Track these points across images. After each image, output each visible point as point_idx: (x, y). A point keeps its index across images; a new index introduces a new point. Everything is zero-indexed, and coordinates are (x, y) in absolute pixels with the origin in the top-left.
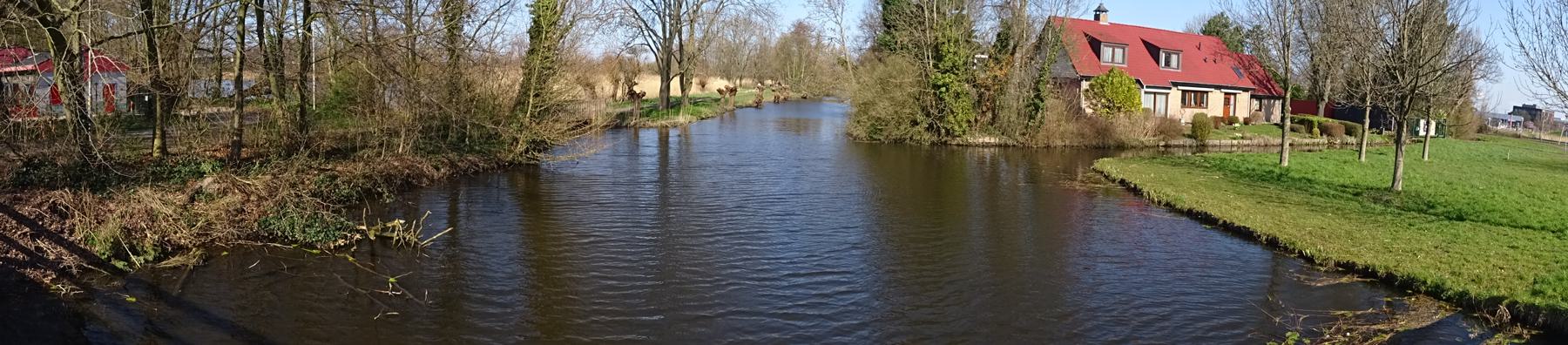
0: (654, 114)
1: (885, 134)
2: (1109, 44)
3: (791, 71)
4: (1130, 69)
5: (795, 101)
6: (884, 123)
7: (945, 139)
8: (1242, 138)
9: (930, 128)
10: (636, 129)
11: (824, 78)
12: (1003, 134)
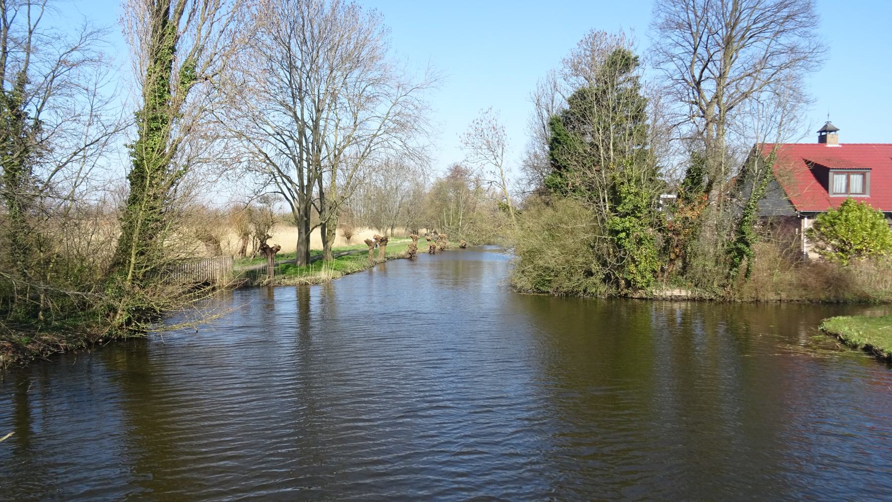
0: (292, 270)
1: (555, 285)
2: (840, 171)
3: (448, 218)
4: (874, 200)
5: (452, 252)
6: (553, 274)
7: (626, 291)
9: (607, 279)
10: (270, 288)
11: (484, 225)
12: (696, 286)
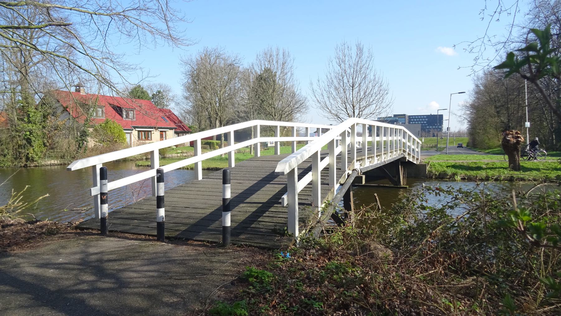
8: (181, 153)
